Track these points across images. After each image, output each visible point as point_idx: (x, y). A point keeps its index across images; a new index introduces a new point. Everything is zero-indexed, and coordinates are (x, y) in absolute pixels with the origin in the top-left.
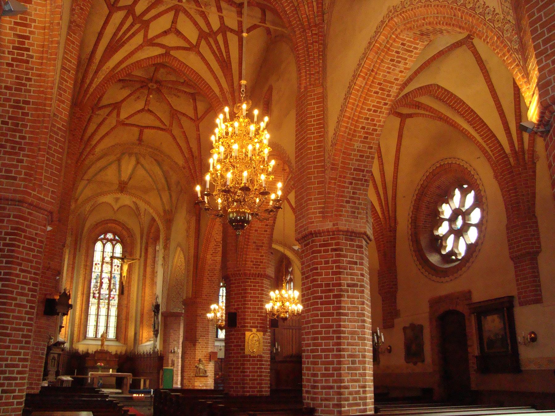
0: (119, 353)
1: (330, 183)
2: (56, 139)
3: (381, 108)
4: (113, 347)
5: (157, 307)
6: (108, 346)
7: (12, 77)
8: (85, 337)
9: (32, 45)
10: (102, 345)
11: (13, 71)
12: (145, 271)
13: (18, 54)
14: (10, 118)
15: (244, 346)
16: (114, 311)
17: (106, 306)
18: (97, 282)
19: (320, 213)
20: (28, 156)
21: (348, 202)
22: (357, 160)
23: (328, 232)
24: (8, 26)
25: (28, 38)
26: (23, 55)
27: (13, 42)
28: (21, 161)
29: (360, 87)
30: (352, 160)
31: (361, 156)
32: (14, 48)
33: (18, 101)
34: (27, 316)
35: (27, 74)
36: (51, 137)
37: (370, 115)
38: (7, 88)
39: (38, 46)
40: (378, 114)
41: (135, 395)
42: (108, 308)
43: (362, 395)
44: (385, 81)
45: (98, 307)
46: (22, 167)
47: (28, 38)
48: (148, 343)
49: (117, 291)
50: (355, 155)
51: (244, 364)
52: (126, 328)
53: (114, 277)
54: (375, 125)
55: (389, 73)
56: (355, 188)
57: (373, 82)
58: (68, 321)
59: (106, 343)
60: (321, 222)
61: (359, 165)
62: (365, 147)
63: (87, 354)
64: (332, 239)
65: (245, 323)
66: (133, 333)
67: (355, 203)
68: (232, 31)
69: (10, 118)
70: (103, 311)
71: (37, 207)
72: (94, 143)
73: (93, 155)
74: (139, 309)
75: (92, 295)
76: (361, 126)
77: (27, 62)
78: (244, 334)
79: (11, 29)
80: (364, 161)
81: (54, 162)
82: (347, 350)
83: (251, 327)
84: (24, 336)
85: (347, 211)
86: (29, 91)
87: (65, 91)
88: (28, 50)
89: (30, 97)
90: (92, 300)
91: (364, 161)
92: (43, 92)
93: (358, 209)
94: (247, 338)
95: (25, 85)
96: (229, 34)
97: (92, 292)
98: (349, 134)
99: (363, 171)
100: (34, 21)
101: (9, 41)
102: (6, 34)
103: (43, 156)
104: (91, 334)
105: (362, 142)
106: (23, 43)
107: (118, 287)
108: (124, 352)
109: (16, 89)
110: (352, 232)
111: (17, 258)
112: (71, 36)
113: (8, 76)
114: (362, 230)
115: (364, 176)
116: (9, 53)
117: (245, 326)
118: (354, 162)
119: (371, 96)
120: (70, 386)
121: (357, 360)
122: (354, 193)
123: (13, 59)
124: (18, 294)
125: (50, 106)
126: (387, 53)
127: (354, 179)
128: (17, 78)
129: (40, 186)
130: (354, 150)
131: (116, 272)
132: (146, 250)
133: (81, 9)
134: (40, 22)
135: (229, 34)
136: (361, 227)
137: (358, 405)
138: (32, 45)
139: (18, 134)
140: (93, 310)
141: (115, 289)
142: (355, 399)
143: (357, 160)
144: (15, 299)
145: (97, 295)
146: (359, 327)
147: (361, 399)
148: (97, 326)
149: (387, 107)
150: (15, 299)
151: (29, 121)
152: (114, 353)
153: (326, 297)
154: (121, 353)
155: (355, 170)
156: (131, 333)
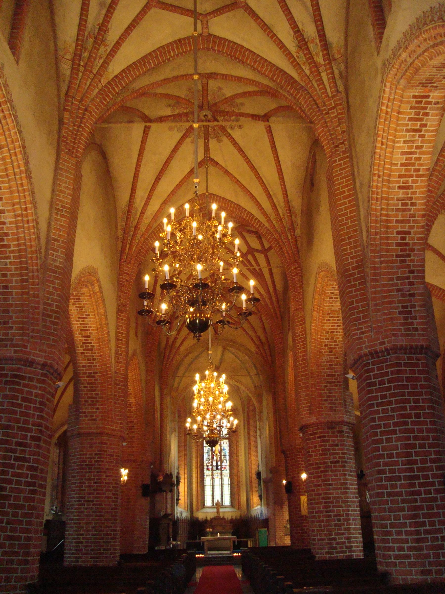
0: (234, 518)
1: (312, 387)
2: (119, 388)
3: (337, 329)
4: (228, 513)
5: (259, 474)
6: (224, 512)
7: (85, 360)
8: (203, 506)
9: (93, 340)
10: (218, 512)
11: (85, 356)
12: (249, 441)
13: (86, 346)
14: (88, 384)
15: (300, 507)
16: (227, 480)
17: (220, 477)
18: (209, 456)
19: (308, 410)
20: (101, 405)
21: (326, 400)
22: (327, 369)
23: (314, 424)
24: (77, 332)
25: (89, 337)
26: (88, 346)
27: (82, 340)
28: (98, 409)
29: (316, 317)
30: (323, 369)
31: (330, 365)
32: (83, 343)
33: (91, 373)
34: (113, 504)
35: (93, 356)
36: (115, 388)
37: (330, 336)
38: (83, 366)
39: (96, 339)
40: (335, 333)
41: (235, 554)
42: (222, 478)
43: (347, 545)
44: (331, 311)
45: (213, 478)
46: (99, 412)
47: (89, 337)
48: (258, 509)
49: (228, 462)
50: (325, 366)
51: (302, 523)
52: (239, 495)
53: (224, 449)
54: (335, 342)
55: (333, 306)
56: (330, 389)
57: (323, 314)
58: (186, 493)
59: (221, 510)
60: (309, 417)
61: (330, 372)
62: (332, 358)
63: (206, 520)
64: (318, 429)
65: (299, 489)
66: (245, 499)
67: (332, 400)
68: (257, 251)
69: (88, 384)
70: (217, 481)
71: (112, 436)
72: (177, 345)
73: (179, 355)
74: (248, 476)
75: (205, 467)
76: (324, 344)
77: (92, 350)
78: (300, 499)
79: (79, 334)
80: (334, 368)
81: (119, 404)
82: (333, 511)
83: (305, 492)
84: (112, 516)
85: (326, 407)
86: (95, 366)
87: (121, 354)
88: (91, 343)
89: (97, 369)
90: (206, 472)
91: (334, 368)
92: (104, 365)
93: (335, 404)
94: (302, 501)
95: (93, 363)
96: (256, 254)
97: (205, 464)
98: (317, 351)
99: (334, 375)
100: (91, 327)
101: (80, 340)
102: (78, 337)
103: (111, 402)
104: (208, 502)
105: (328, 355)
106: (87, 340)
107: (228, 457)
108: (238, 518)
109: (89, 366)
110: (332, 422)
111: (103, 468)
112: (120, 316)
113: (82, 360)
114: (340, 420)
115: (337, 379)
116: (81, 347)
117: (300, 492)
118: (326, 370)
119: (325, 323)
120: (318, 557)
121: (342, 518)
122: (330, 393)
123: (84, 350)
124: (106, 490)
125: (111, 370)
126: (325, 295)
127: (328, 382)
128: (88, 360)
129: (111, 422)
130: (324, 362)
131: (225, 444)
132: (248, 421)
133: (125, 293)
134: (94, 327)
135: (256, 254)
136: (339, 417)
137: (345, 552)
138: (93, 340)
139: (94, 393)
140: (208, 481)
141: (226, 460)
142: (342, 548)
143: (327, 369)
144: (105, 494)
145: (210, 467)
146: (342, 493)
147: (346, 547)
148: (213, 495)
149: (341, 327)
150: (105, 494)
151: (99, 383)
152: (230, 518)
153: (316, 473)
154: (236, 518)
155: (327, 376)
156: (243, 499)
